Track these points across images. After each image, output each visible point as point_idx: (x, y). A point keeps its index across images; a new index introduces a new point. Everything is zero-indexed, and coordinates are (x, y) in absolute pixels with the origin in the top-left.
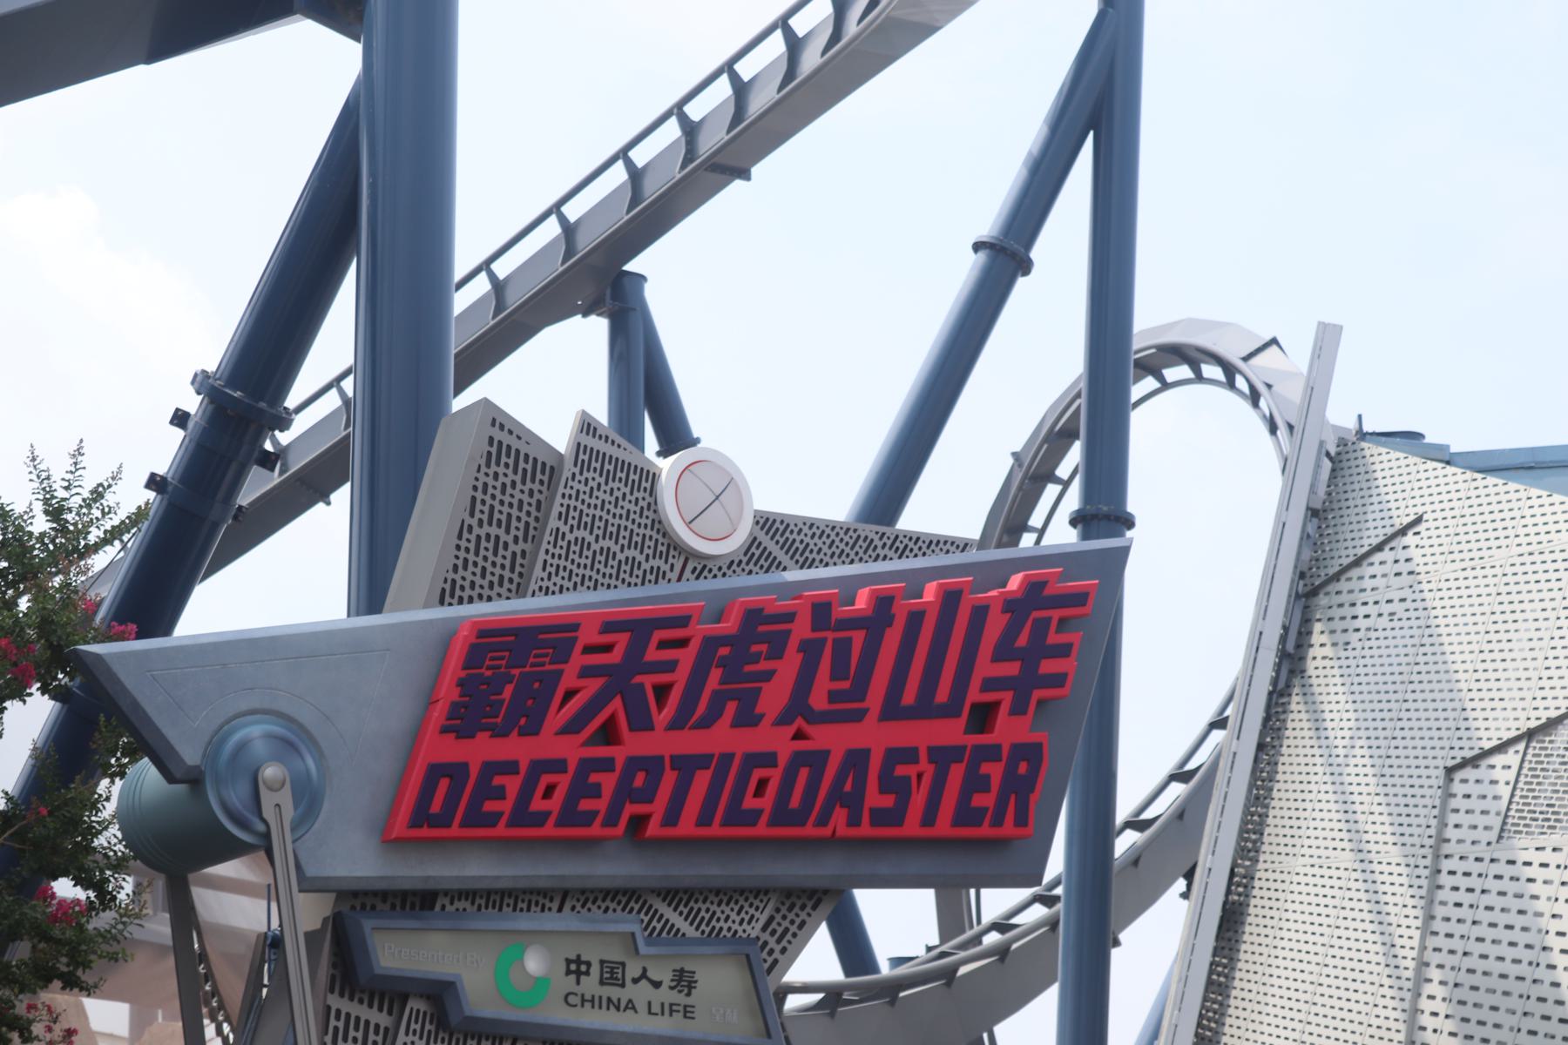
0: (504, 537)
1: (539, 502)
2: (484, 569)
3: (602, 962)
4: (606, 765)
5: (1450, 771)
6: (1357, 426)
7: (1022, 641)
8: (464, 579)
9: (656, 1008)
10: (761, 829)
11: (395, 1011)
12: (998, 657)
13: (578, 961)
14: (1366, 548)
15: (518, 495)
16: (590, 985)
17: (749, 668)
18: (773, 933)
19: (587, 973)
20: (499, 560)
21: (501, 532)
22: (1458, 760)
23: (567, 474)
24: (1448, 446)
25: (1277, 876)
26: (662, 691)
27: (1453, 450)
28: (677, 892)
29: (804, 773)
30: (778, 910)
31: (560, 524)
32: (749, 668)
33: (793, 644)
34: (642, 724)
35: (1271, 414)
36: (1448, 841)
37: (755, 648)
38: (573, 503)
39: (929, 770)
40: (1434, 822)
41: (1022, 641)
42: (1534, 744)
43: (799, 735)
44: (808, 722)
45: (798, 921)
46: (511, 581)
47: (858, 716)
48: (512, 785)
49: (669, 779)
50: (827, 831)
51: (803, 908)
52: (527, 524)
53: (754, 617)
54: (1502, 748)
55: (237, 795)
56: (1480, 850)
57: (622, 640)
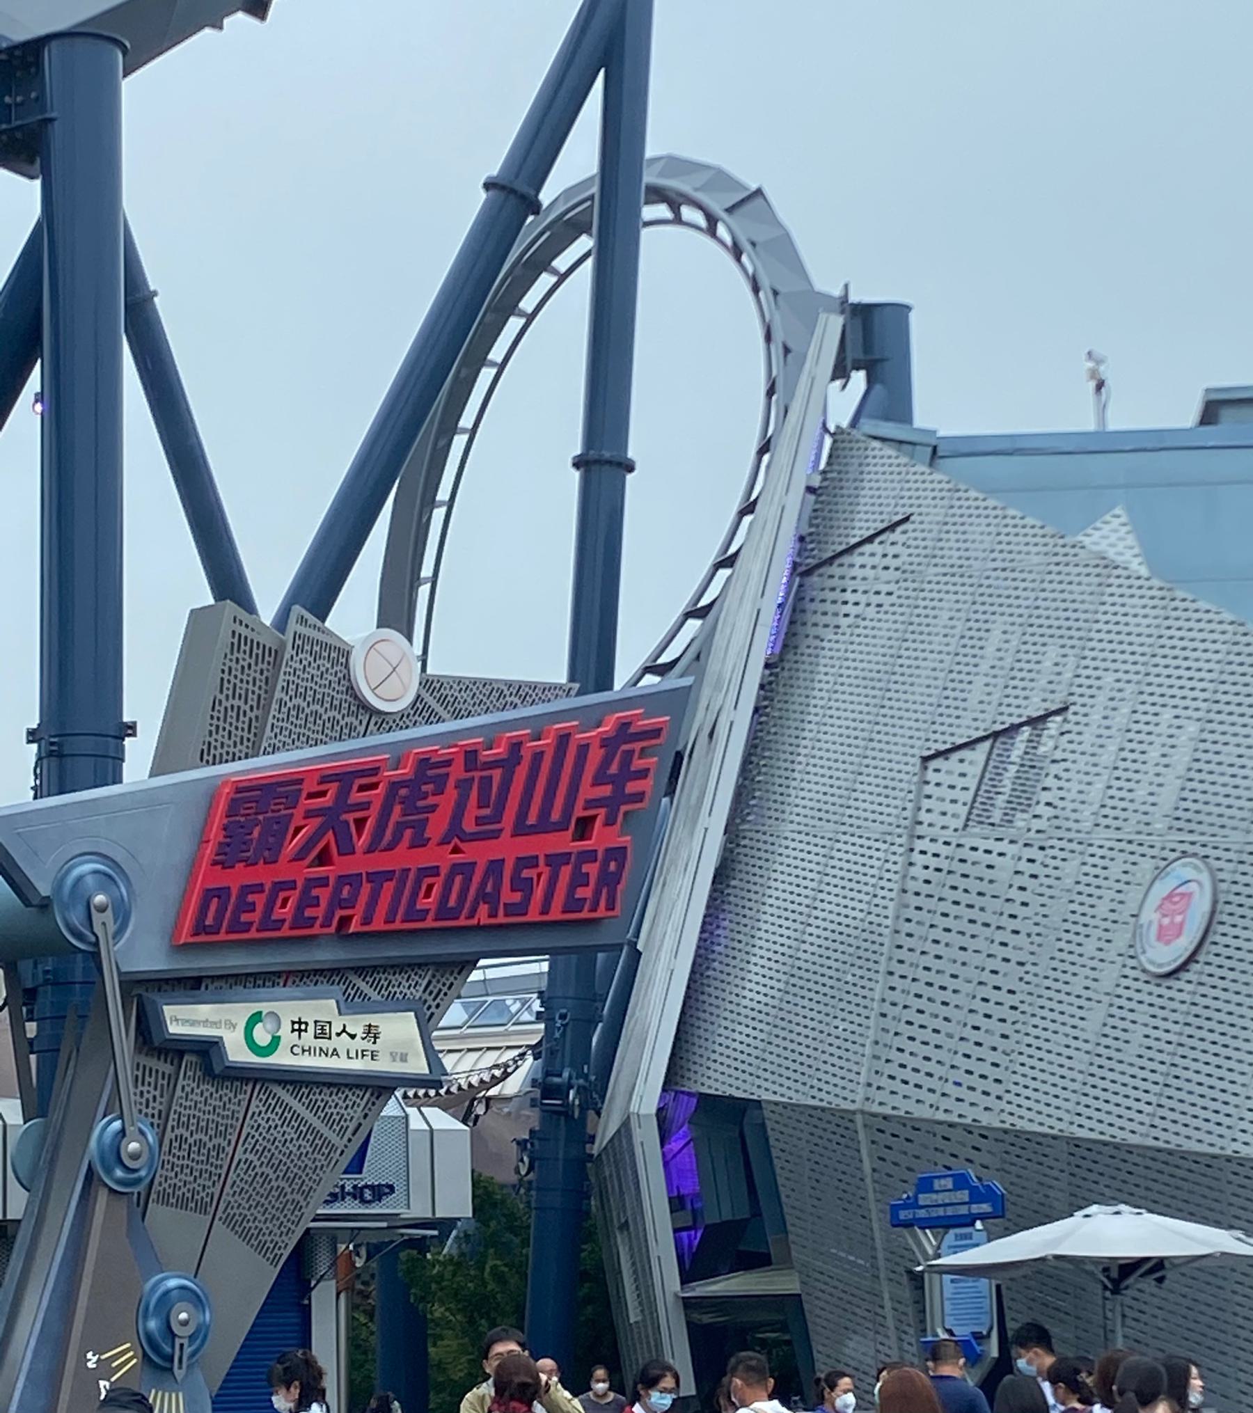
0: (243, 707)
1: (267, 678)
2: (230, 732)
3: (316, 1022)
4: (323, 882)
5: (926, 759)
6: (843, 293)
7: (614, 769)
8: (216, 740)
9: (353, 1054)
10: (429, 923)
11: (176, 1062)
12: (595, 784)
13: (300, 1023)
14: (857, 540)
15: (253, 674)
16: (308, 1038)
17: (420, 804)
18: (431, 993)
19: (306, 1030)
20: (240, 725)
21: (241, 703)
22: (932, 752)
23: (287, 656)
24: (935, 432)
25: (771, 839)
26: (360, 823)
27: (941, 433)
28: (364, 968)
29: (458, 879)
30: (434, 976)
31: (283, 695)
32: (420, 804)
33: (451, 783)
34: (348, 850)
35: (755, 270)
36: (920, 823)
37: (424, 788)
38: (291, 678)
39: (546, 871)
40: (909, 806)
41: (614, 769)
42: (998, 744)
43: (456, 850)
44: (462, 841)
45: (448, 983)
46: (248, 740)
47: (495, 835)
48: (259, 900)
49: (366, 888)
50: (474, 922)
51: (452, 974)
52: (259, 696)
53: (424, 763)
54: (971, 744)
55: (76, 918)
56: (948, 835)
57: (332, 789)
